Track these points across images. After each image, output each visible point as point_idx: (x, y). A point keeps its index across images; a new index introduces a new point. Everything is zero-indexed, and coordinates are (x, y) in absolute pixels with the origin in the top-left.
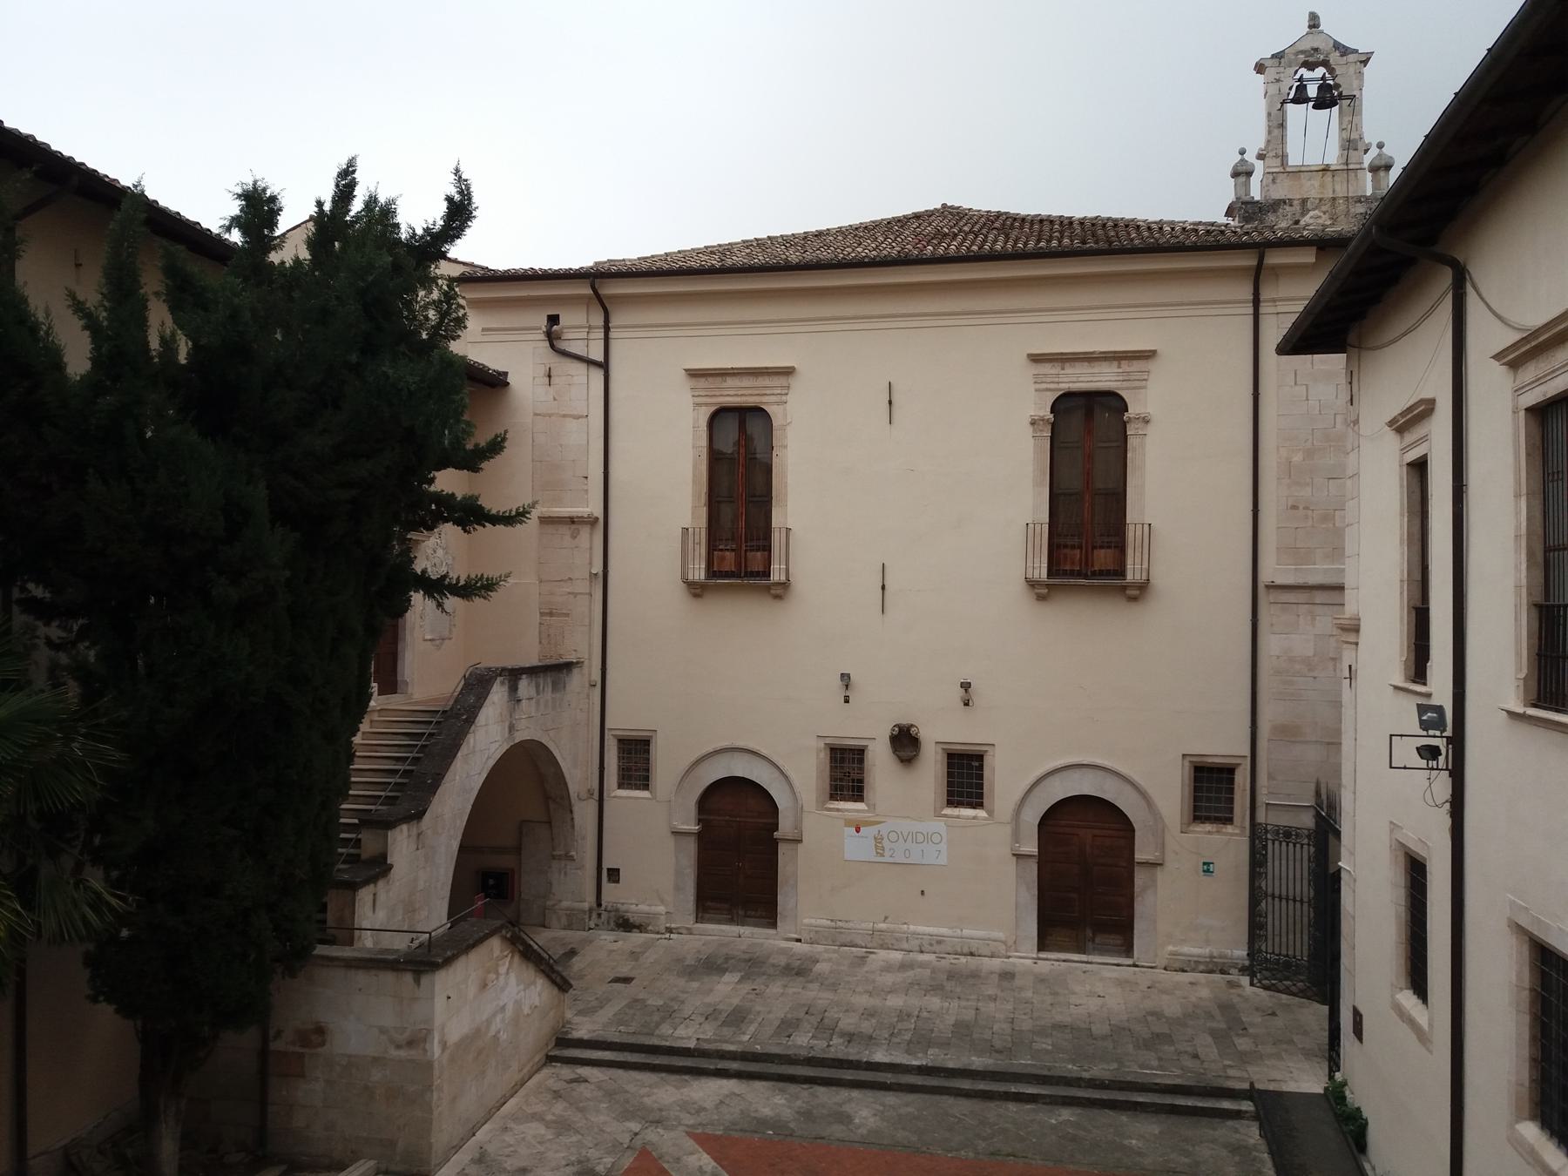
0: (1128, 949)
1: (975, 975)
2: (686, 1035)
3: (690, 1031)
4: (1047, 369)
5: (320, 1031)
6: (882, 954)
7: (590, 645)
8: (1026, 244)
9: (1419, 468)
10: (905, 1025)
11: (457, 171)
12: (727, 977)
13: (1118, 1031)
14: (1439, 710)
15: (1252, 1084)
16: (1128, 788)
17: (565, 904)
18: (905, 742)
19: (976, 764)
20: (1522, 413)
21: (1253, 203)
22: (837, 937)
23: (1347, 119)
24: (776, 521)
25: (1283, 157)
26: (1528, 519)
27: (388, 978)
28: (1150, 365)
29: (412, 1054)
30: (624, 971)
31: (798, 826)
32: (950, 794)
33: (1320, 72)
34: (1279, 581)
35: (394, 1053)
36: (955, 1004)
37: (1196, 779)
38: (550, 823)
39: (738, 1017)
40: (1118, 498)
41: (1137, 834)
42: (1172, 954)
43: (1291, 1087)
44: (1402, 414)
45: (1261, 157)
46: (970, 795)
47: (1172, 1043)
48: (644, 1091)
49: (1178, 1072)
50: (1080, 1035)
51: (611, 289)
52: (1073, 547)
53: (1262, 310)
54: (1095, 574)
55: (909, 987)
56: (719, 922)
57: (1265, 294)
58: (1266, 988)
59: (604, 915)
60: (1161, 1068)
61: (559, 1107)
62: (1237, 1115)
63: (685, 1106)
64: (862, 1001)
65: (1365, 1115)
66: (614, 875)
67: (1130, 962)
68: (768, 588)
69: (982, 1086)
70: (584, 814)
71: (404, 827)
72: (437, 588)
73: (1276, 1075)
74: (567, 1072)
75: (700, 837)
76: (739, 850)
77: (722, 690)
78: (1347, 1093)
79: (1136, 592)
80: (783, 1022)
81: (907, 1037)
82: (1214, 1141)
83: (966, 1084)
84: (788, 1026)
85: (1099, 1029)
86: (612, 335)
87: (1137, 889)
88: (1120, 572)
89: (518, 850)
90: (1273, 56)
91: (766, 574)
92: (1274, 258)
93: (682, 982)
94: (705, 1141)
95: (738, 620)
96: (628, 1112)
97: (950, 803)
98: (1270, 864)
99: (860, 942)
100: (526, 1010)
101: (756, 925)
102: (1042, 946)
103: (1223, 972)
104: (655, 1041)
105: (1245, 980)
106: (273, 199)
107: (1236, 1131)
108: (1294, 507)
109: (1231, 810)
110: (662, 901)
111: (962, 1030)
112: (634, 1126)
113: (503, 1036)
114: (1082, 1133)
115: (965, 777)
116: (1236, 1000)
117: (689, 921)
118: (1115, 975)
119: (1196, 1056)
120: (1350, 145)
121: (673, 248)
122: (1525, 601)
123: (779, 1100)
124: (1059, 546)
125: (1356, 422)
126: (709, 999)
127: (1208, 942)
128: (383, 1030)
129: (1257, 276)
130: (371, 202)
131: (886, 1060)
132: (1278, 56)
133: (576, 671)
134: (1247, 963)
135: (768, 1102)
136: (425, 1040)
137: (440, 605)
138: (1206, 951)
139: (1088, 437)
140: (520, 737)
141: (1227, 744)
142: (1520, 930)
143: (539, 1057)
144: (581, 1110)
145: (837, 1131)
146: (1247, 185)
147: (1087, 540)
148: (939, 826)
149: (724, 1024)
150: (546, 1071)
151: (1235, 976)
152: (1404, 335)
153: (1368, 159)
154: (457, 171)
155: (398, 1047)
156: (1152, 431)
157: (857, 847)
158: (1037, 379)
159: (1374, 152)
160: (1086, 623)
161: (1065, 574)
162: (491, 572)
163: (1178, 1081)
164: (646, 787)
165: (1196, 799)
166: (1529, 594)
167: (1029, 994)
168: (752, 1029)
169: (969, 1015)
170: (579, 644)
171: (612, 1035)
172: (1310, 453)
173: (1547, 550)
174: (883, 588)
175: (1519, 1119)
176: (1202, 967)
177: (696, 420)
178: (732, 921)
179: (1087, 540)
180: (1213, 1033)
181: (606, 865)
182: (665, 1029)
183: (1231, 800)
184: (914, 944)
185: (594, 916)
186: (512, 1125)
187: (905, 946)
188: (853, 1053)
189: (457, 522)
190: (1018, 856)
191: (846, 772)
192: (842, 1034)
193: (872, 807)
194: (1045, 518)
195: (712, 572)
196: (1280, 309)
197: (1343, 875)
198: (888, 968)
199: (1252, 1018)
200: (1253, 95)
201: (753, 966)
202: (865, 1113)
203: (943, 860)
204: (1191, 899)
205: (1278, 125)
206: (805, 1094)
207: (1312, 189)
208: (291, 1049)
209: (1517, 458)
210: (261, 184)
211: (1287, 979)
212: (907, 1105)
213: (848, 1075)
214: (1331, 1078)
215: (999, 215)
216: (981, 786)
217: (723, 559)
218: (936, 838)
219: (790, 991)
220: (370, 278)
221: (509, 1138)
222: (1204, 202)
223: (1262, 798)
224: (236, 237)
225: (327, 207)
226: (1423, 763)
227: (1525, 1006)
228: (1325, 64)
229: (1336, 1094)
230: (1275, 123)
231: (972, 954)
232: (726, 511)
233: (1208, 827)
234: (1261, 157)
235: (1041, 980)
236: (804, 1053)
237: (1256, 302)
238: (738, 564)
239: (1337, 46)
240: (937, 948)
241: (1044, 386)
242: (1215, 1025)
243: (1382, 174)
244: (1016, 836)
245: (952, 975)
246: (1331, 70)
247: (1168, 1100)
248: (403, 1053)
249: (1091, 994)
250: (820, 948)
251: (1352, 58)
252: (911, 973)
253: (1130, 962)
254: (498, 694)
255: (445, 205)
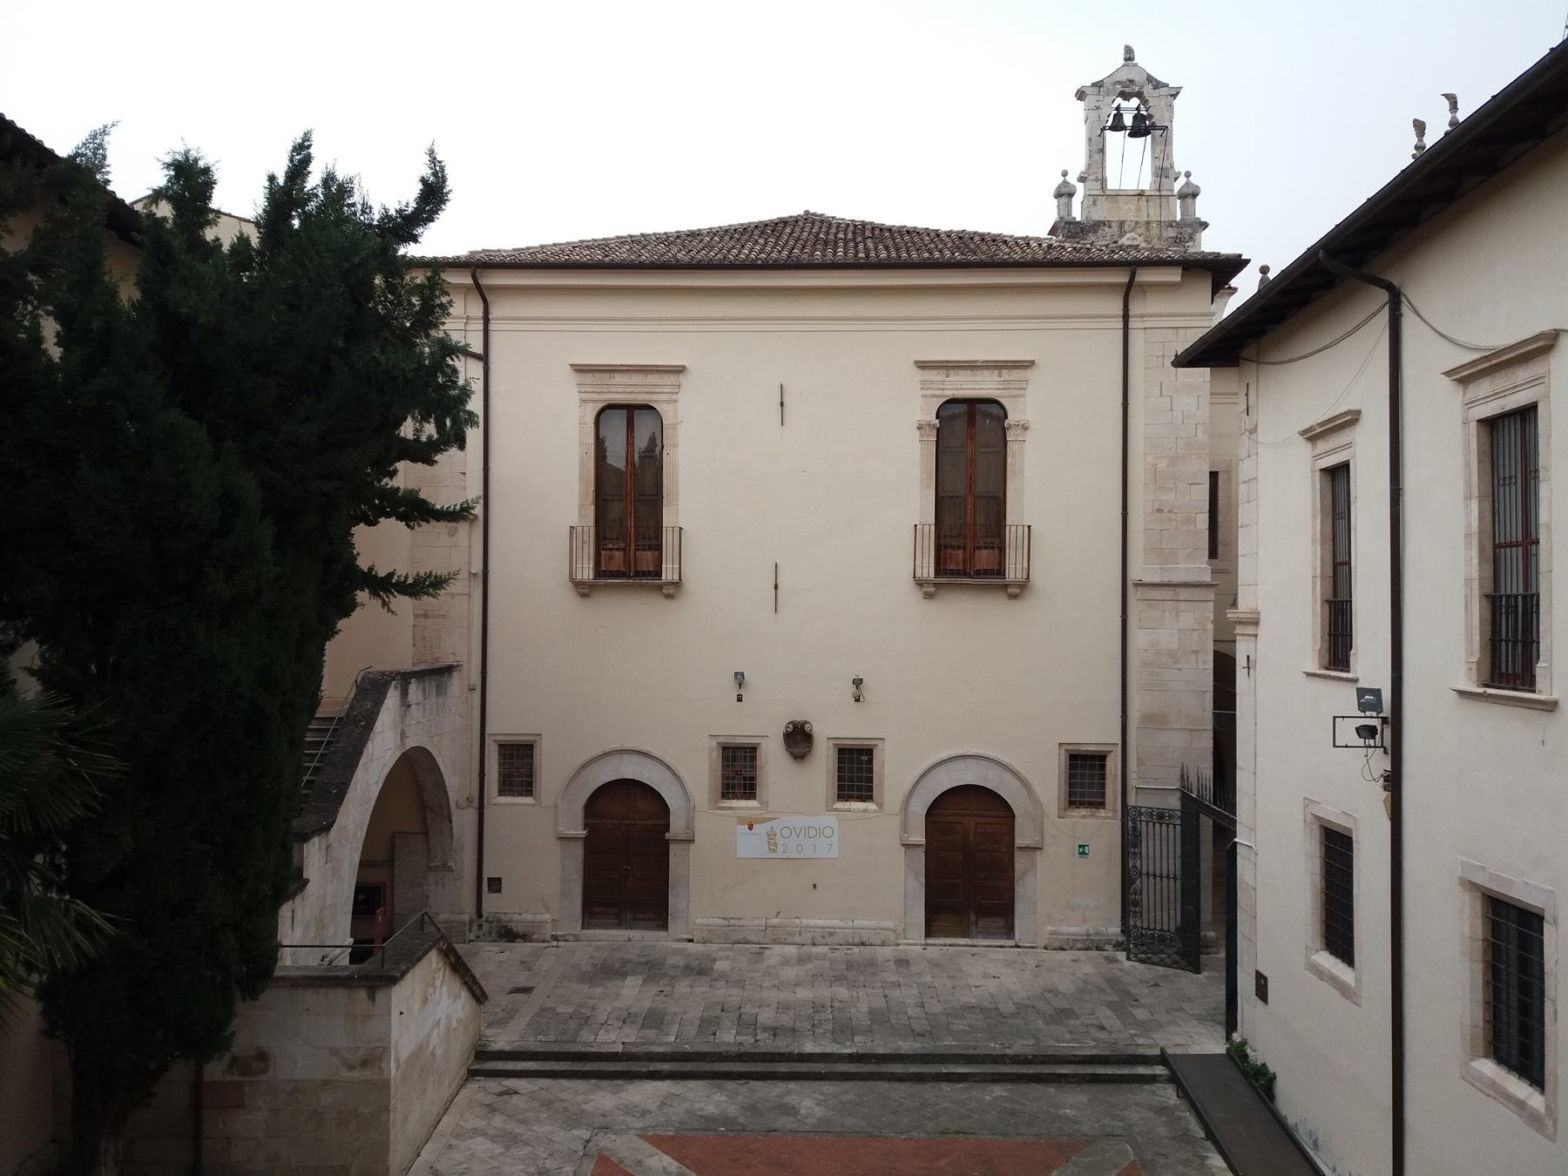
0: (1009, 931)
1: (872, 963)
2: (611, 1039)
3: (613, 1036)
4: (932, 375)
5: (262, 1056)
6: (777, 949)
7: (469, 650)
8: (835, 253)
9: (1337, 476)
10: (823, 1016)
11: (431, 153)
12: (630, 981)
13: (1023, 1009)
14: (1377, 693)
15: (1162, 1049)
16: (1009, 776)
17: (443, 917)
18: (798, 739)
19: (865, 758)
20: (1473, 425)
21: (1074, 223)
22: (731, 936)
23: (1158, 148)
24: (668, 520)
25: (1103, 181)
26: (1480, 519)
27: (340, 994)
28: (1028, 374)
29: (367, 1074)
30: (522, 980)
31: (690, 826)
32: (840, 788)
33: (1135, 102)
34: (1146, 580)
35: (346, 1074)
36: (862, 993)
37: (1071, 767)
38: (426, 833)
39: (655, 1020)
40: (997, 504)
41: (1018, 821)
42: (1052, 933)
43: (1195, 1050)
44: (1321, 425)
45: (1082, 179)
46: (859, 789)
47: (1077, 1017)
48: (580, 1099)
49: (1092, 1043)
50: (991, 1014)
51: (491, 279)
52: (959, 548)
53: (1131, 325)
54: (979, 573)
55: (816, 977)
56: (606, 927)
57: (1135, 309)
58: (1141, 961)
59: (486, 927)
60: (1074, 1040)
61: (498, 1121)
62: (1153, 1079)
63: (628, 1110)
64: (772, 996)
65: (1271, 1069)
66: (496, 885)
67: (1012, 943)
68: (660, 588)
69: (913, 1069)
70: (463, 821)
71: (316, 839)
72: (383, 586)
73: (1180, 1040)
74: (493, 1085)
75: (587, 842)
76: (628, 853)
77: (608, 688)
78: (1249, 1051)
79: (671, 591)
80: (703, 1021)
81: (830, 1027)
82: (1138, 1105)
83: (898, 1068)
84: (708, 1025)
85: (1007, 1008)
86: (492, 327)
87: (1017, 874)
88: (1000, 572)
89: (391, 863)
90: (1094, 85)
91: (658, 573)
92: (1144, 276)
93: (585, 988)
94: (662, 1142)
95: (628, 616)
96: (572, 1119)
97: (841, 797)
98: (1144, 844)
99: (751, 937)
100: (454, 1025)
101: (644, 928)
102: (929, 933)
103: (1098, 949)
104: (581, 1049)
105: (1121, 956)
106: (207, 171)
107: (1155, 1094)
108: (1160, 511)
109: (1103, 795)
110: (547, 909)
111: (879, 1018)
112: (586, 1134)
113: (439, 1052)
114: (1018, 1107)
115: (856, 772)
116: (1119, 974)
117: (576, 928)
118: (1001, 956)
119: (1102, 1028)
120: (1163, 172)
121: (535, 242)
122: (1476, 592)
123: (720, 1097)
124: (946, 547)
125: (1254, 431)
126: (618, 1004)
127: (1084, 920)
128: (333, 1051)
129: (1128, 291)
130: (329, 179)
131: (818, 1050)
132: (1098, 85)
133: (455, 674)
134: (1120, 939)
135: (708, 1100)
136: (380, 1059)
137: (385, 604)
138: (1083, 930)
139: (971, 439)
140: (411, 743)
141: (1098, 732)
142: (1474, 886)
143: (463, 1071)
144: (522, 1122)
145: (786, 1122)
146: (1069, 206)
147: (970, 540)
148: (831, 820)
149: (643, 1027)
150: (472, 1086)
151: (1110, 951)
152: (1312, 354)
153: (1178, 185)
154: (431, 153)
155: (352, 1068)
156: (1029, 436)
157: (749, 845)
158: (924, 385)
159: (1182, 181)
160: (970, 617)
161: (952, 573)
162: (440, 570)
163: (1094, 1052)
164: (529, 793)
165: (1071, 785)
166: (1481, 586)
167: (929, 979)
168: (674, 1029)
169: (880, 1003)
170: (459, 646)
171: (532, 1044)
172: (1174, 460)
173: (1495, 547)
174: (776, 587)
175: (1474, 1057)
176: (1079, 945)
177: (582, 417)
178: (621, 924)
179: (970, 540)
180: (1109, 1005)
181: (486, 875)
182: (586, 1036)
183: (1103, 786)
184: (807, 937)
185: (475, 926)
186: (454, 1142)
187: (798, 939)
188: (782, 1045)
189: (400, 518)
190: (907, 846)
191: (738, 771)
192: (765, 1029)
193: (765, 804)
194: (931, 518)
195: (599, 573)
196: (1147, 325)
197: (1239, 849)
198: (786, 962)
199: (1141, 991)
200: (1073, 122)
201: (652, 969)
202: (807, 1103)
203: (834, 853)
204: (1068, 877)
205: (1097, 151)
206: (743, 1089)
207: (1128, 212)
208: (228, 1078)
209: (1467, 464)
210: (193, 154)
211: (1162, 952)
212: (846, 1092)
213: (783, 1068)
214: (1229, 1038)
215: (864, 224)
216: (871, 780)
217: (611, 558)
218: (828, 832)
219: (699, 990)
220: (357, 259)
221: (457, 1156)
222: (1029, 218)
223: (1133, 781)
224: (164, 210)
225: (281, 181)
226: (1361, 742)
227: (1478, 955)
228: (1139, 95)
229: (1238, 1054)
230: (1095, 148)
231: (863, 944)
232: (615, 510)
233: (1083, 811)
234: (1082, 179)
235: (934, 964)
236: (735, 1049)
237: (1126, 317)
238: (626, 561)
239: (1150, 79)
240: (829, 940)
241: (930, 392)
242: (1108, 998)
243: (1189, 200)
244: (905, 827)
245: (850, 965)
246: (1144, 101)
247: (1089, 1070)
248: (355, 1074)
249: (986, 976)
250: (714, 947)
251: (1163, 91)
252: (809, 966)
253: (1012, 943)
254: (392, 699)
255: (420, 186)
